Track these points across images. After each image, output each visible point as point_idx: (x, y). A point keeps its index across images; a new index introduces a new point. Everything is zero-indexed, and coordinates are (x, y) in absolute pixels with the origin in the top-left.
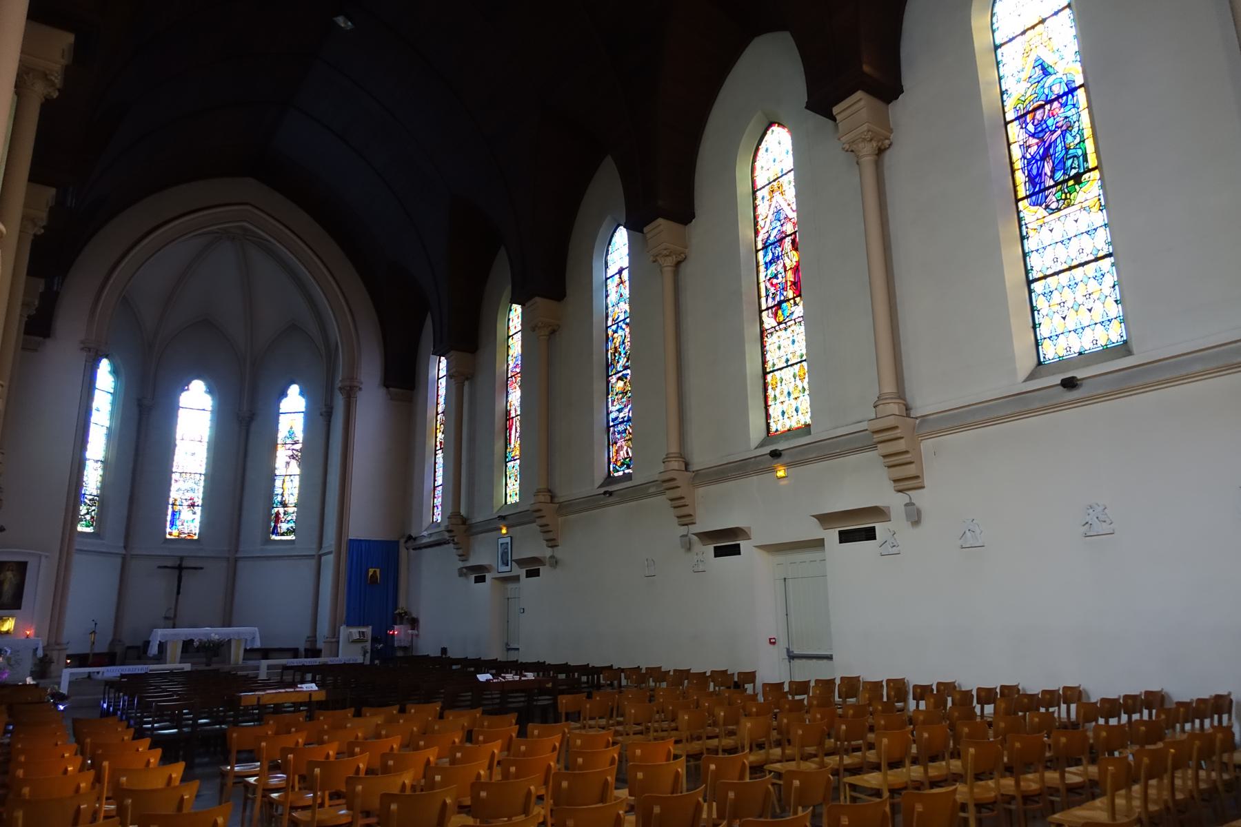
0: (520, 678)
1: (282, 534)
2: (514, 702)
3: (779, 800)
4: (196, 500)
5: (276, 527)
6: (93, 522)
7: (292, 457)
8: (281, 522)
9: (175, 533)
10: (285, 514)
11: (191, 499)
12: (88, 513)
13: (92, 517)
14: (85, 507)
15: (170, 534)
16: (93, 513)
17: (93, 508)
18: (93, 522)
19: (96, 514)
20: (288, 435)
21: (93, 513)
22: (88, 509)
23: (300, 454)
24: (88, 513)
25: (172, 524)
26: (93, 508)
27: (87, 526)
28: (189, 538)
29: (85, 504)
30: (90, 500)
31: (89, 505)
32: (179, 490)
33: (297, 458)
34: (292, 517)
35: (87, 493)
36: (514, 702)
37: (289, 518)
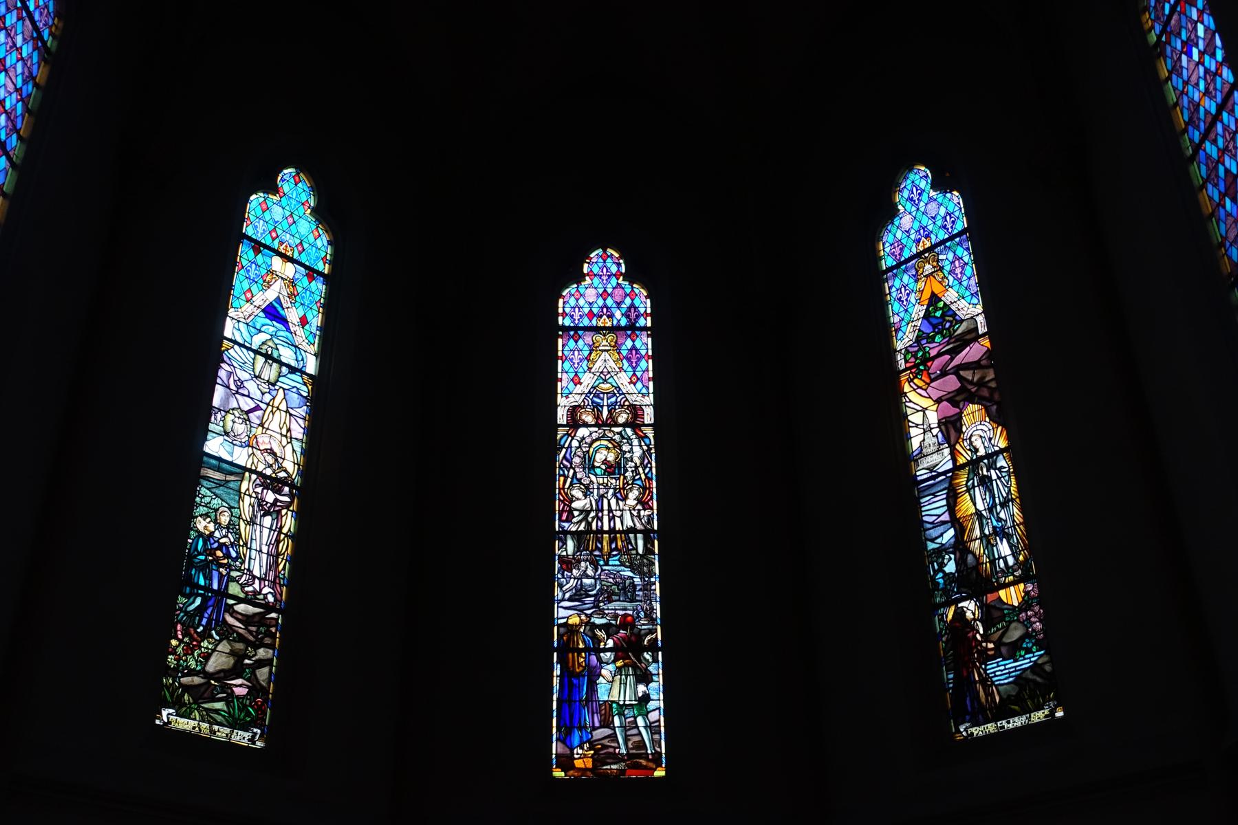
0: (203, 626)
1: (1003, 712)
2: (1026, 663)
3: (243, 554)
4: (643, 625)
5: (965, 685)
6: (260, 710)
7: (958, 399)
8: (986, 657)
9: (583, 760)
10: (988, 620)
11: (623, 625)
12: (236, 671)
13: (256, 689)
14: (224, 647)
15: (566, 762)
16: (263, 674)
17: (262, 653)
18: (260, 710)
19: (277, 678)
20: (927, 329)
21: (263, 674)
22: (238, 656)
23: (991, 375)
24: (236, 671)
25: (570, 724)
26: (262, 653)
27: (234, 724)
28: (633, 775)
29: (227, 632)
30: (246, 620)
31: (241, 638)
32: (579, 594)
33: (985, 393)
34: (1027, 623)
35: (234, 589)
36: (1026, 663)
37: (1015, 633)
